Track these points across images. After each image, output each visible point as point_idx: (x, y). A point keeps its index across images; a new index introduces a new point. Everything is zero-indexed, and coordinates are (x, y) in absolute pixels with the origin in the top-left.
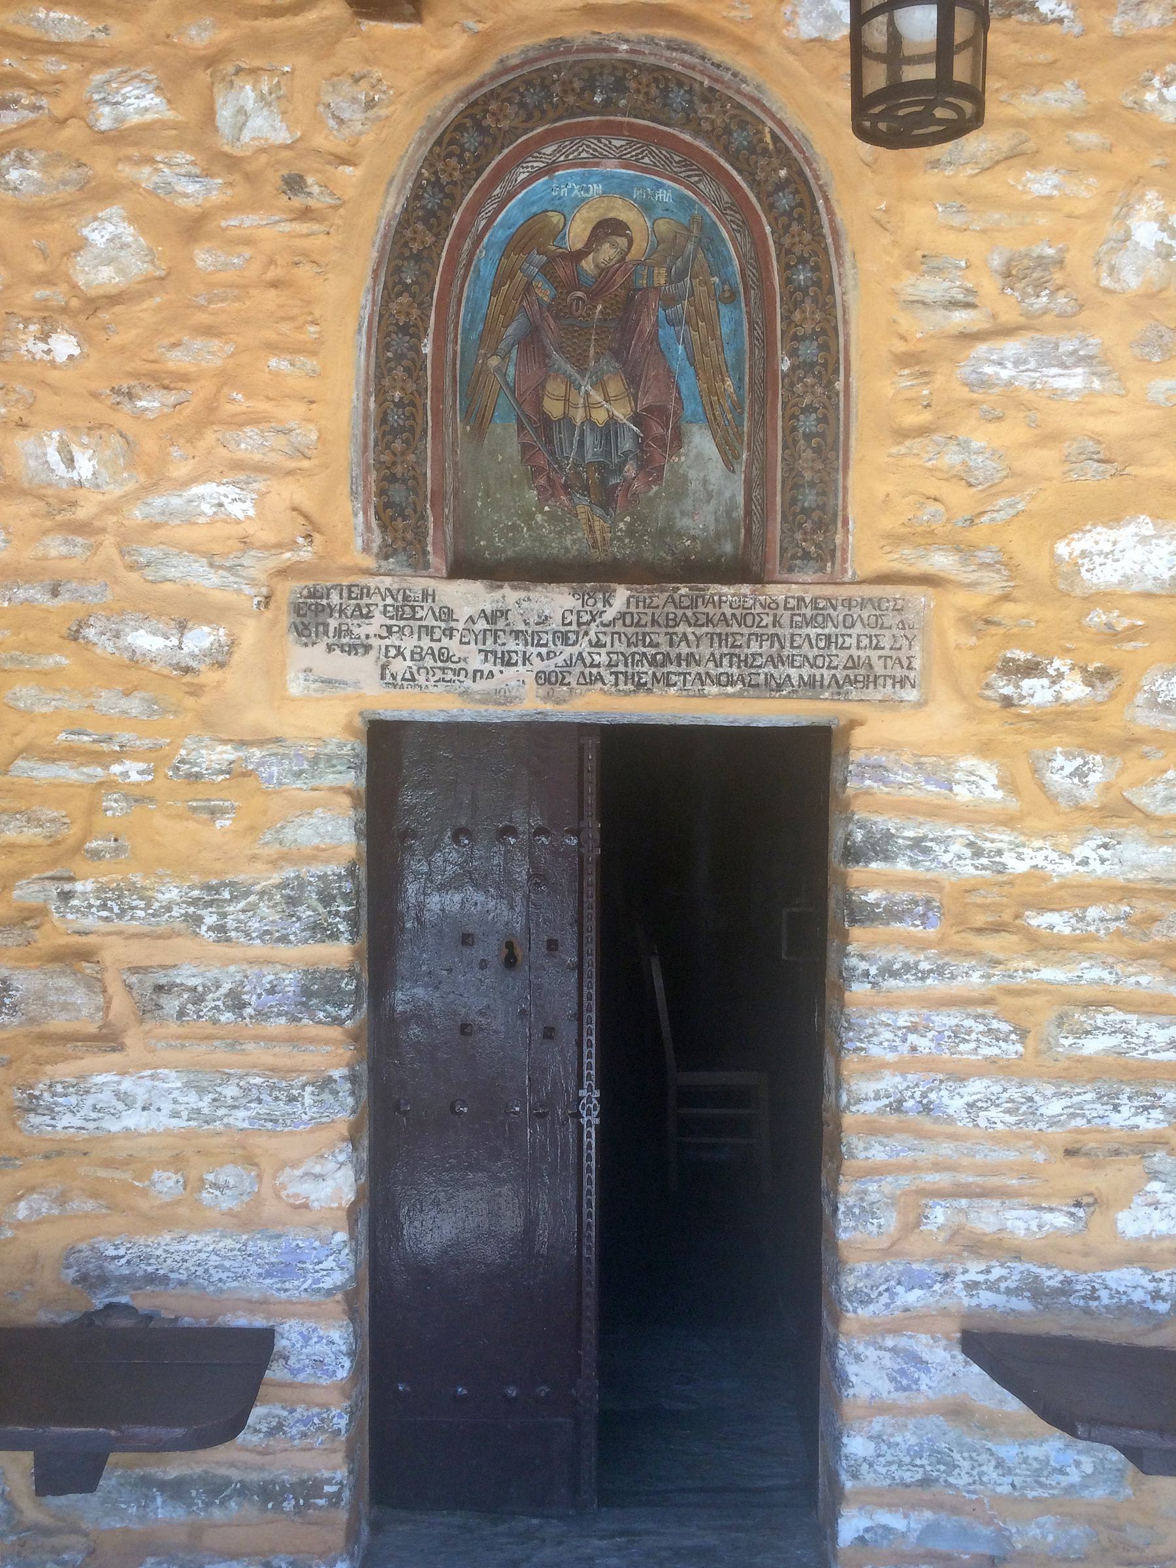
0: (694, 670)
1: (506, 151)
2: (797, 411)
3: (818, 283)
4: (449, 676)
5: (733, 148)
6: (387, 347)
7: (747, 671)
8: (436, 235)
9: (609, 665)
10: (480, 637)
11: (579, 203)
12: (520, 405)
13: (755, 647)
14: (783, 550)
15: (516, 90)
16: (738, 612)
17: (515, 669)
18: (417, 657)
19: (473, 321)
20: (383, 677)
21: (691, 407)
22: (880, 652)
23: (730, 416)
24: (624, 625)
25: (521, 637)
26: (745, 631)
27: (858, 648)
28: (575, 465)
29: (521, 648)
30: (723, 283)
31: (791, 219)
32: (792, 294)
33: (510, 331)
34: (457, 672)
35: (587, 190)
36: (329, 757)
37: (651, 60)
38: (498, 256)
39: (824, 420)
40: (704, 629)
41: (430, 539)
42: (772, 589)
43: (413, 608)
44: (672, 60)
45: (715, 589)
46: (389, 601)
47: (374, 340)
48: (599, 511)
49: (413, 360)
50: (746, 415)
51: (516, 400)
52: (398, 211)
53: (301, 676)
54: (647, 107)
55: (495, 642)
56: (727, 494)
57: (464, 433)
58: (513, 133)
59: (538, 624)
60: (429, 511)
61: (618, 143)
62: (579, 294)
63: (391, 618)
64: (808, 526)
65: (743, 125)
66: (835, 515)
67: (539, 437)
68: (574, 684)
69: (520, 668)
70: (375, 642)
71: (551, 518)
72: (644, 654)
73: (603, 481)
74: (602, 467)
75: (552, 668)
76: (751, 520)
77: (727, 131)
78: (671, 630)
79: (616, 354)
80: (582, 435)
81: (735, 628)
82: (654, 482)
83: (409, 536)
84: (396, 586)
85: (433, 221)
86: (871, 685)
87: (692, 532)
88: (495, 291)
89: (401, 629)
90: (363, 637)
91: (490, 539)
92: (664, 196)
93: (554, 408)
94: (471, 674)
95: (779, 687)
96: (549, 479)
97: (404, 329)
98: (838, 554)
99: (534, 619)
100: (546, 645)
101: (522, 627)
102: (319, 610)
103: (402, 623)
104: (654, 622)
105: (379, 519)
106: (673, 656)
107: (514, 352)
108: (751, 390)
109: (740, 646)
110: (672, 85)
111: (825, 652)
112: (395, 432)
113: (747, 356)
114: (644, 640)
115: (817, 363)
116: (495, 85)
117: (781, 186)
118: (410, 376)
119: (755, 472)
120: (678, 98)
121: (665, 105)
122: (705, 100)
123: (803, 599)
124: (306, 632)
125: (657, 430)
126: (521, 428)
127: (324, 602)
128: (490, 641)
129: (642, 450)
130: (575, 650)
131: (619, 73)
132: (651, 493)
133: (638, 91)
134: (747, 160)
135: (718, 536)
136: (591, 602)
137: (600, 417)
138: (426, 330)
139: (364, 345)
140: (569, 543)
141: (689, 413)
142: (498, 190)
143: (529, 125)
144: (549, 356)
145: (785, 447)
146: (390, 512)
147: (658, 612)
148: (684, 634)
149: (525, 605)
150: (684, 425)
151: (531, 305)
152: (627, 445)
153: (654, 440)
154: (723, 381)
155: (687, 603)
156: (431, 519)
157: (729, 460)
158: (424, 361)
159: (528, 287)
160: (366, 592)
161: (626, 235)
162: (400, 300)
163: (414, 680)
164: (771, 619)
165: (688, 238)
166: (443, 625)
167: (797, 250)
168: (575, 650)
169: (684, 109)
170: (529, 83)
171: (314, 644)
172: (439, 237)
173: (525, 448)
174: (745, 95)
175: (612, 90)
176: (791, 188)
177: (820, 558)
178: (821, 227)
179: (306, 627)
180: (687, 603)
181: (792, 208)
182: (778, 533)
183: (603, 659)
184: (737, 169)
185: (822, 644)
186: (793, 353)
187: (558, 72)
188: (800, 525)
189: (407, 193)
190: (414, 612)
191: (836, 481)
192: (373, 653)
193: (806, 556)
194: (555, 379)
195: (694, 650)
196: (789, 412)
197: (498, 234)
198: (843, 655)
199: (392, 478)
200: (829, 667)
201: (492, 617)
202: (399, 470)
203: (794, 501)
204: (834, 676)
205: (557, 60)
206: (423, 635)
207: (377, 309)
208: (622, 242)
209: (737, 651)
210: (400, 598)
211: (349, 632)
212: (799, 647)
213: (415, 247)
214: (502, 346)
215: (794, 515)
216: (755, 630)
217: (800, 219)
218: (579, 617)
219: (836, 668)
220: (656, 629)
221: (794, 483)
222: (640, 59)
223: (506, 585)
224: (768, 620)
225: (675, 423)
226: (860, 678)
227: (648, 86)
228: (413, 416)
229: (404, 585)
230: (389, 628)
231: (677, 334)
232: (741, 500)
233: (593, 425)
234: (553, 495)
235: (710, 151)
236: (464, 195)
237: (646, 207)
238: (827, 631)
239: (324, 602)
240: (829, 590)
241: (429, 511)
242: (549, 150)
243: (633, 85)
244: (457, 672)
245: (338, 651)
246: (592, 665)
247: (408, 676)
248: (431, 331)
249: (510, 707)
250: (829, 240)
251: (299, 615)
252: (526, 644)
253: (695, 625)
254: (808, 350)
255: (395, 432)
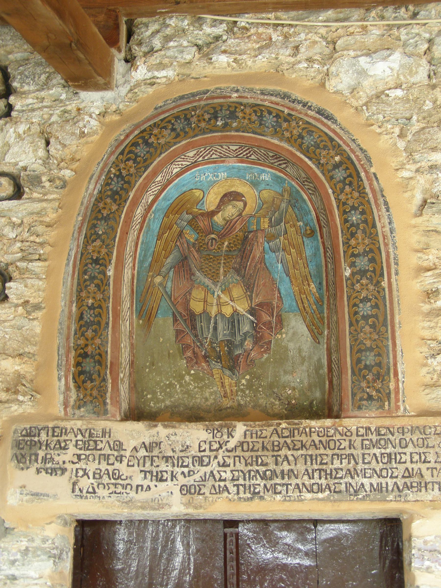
0: (294, 481)
1: (163, 155)
2: (357, 301)
3: (365, 222)
4: (120, 489)
5: (304, 146)
6: (85, 272)
7: (331, 482)
8: (119, 205)
9: (233, 480)
10: (141, 461)
11: (212, 184)
12: (174, 305)
13: (337, 464)
14: (354, 395)
15: (169, 122)
16: (324, 439)
17: (165, 483)
18: (97, 476)
19: (145, 255)
20: (73, 491)
21: (288, 302)
22: (428, 465)
23: (314, 307)
24: (243, 450)
25: (170, 461)
26: (330, 452)
27: (412, 462)
28: (211, 343)
29: (170, 468)
30: (306, 225)
31: (345, 184)
32: (348, 229)
33: (169, 260)
34: (124, 487)
35: (217, 176)
36: (37, 549)
37: (251, 101)
38: (162, 216)
39: (376, 306)
40: (300, 452)
41: (108, 395)
42: (346, 422)
43: (95, 442)
44: (265, 100)
45: (306, 423)
46: (80, 437)
47: (77, 269)
48: (228, 372)
49: (102, 281)
50: (325, 306)
51: (173, 303)
52: (96, 192)
53: (18, 491)
54: (250, 126)
55: (152, 465)
56: (315, 358)
57: (138, 324)
58: (168, 145)
59: (182, 451)
60: (109, 376)
61: (234, 148)
62: (213, 236)
63: (81, 449)
64: (370, 377)
65: (310, 133)
66: (389, 369)
67: (188, 327)
68: (207, 494)
69: (169, 483)
70: (68, 466)
71: (196, 378)
72: (258, 471)
73: (230, 352)
74: (230, 343)
75: (192, 482)
76: (332, 375)
77: (301, 137)
78: (276, 453)
79: (238, 271)
80: (216, 323)
81: (322, 451)
82: (265, 352)
83: (95, 393)
84: (84, 427)
85: (117, 197)
86: (423, 489)
87: (292, 384)
88: (159, 237)
89: (87, 457)
90: (61, 463)
91: (154, 393)
92: (264, 177)
93: (197, 307)
94: (134, 488)
95: (356, 492)
96: (194, 352)
97: (96, 261)
98: (393, 396)
99: (178, 448)
100: (187, 466)
101: (170, 454)
102: (33, 444)
103: (88, 453)
104: (264, 448)
105: (76, 382)
106: (278, 472)
107: (171, 273)
108: (328, 290)
109: (326, 464)
110: (265, 113)
111: (389, 466)
112: (88, 325)
113: (324, 269)
114: (257, 461)
115: (368, 271)
116: (156, 120)
117: (337, 166)
118: (99, 290)
119: (333, 343)
120: (270, 120)
121: (261, 124)
122: (286, 120)
123: (369, 429)
124: (23, 460)
125: (266, 318)
126: (175, 320)
127: (36, 439)
128: (148, 464)
129: (256, 331)
130: (208, 469)
131: (232, 109)
132: (263, 360)
133: (244, 118)
134: (314, 152)
135: (310, 387)
136: (219, 435)
137: (227, 311)
138: (110, 261)
139: (71, 272)
140: (207, 395)
141: (287, 306)
142: (159, 178)
143: (178, 139)
144: (193, 274)
145: (351, 325)
146: (82, 377)
147: (266, 440)
148: (286, 456)
149: (172, 438)
150: (284, 315)
151: (182, 244)
152: (246, 328)
153: (264, 324)
154: (309, 285)
155: (286, 433)
156: (110, 381)
157: (316, 335)
158: (108, 280)
159: (181, 234)
160: (64, 431)
161: (242, 201)
162: (94, 244)
163: (94, 492)
164: (347, 443)
165: (282, 200)
166: (116, 453)
167: (350, 202)
168: (208, 469)
169: (273, 126)
170: (177, 118)
171: (28, 468)
172: (120, 206)
173: (178, 333)
174: (311, 117)
175: (228, 118)
176: (344, 166)
177: (380, 399)
178: (364, 188)
179: (23, 456)
180: (286, 433)
181: (345, 179)
182: (350, 383)
183: (228, 475)
184: (308, 157)
185: (385, 460)
186: (352, 265)
187: (195, 111)
188: (364, 377)
189: (101, 182)
190: (96, 444)
191: (387, 346)
192: (67, 474)
193: (370, 398)
194: (198, 288)
195: (293, 467)
196: (352, 303)
197: (163, 204)
198: (402, 467)
199: (85, 355)
200: (391, 477)
201: (149, 447)
202: (89, 350)
203: (359, 361)
204: (396, 483)
205: (195, 104)
206: (102, 461)
207: (80, 250)
208: (240, 204)
209: (324, 467)
210: (87, 435)
211: (52, 459)
212: (369, 463)
213: (105, 212)
214: (164, 269)
215: (359, 370)
216: (336, 451)
217: (350, 184)
218: (211, 446)
219: (396, 477)
220: (266, 453)
221: (358, 350)
222: (244, 101)
223: (160, 424)
224: (345, 444)
225: (278, 313)
226: (415, 484)
227: (250, 115)
228: (100, 315)
229: (90, 426)
230: (79, 456)
231: (277, 257)
232: (325, 362)
233: (223, 316)
234: (196, 363)
235: (291, 148)
236: (136, 182)
237: (255, 184)
238: (388, 451)
239: (36, 439)
240: (387, 422)
241: (109, 376)
242: (191, 154)
243: (241, 115)
244: (124, 487)
245: (44, 473)
246: (220, 480)
247: (91, 490)
248: (113, 261)
249: (162, 512)
250: (370, 196)
251: (19, 449)
252: (174, 466)
253: (294, 449)
254: (362, 263)
255: (88, 325)
